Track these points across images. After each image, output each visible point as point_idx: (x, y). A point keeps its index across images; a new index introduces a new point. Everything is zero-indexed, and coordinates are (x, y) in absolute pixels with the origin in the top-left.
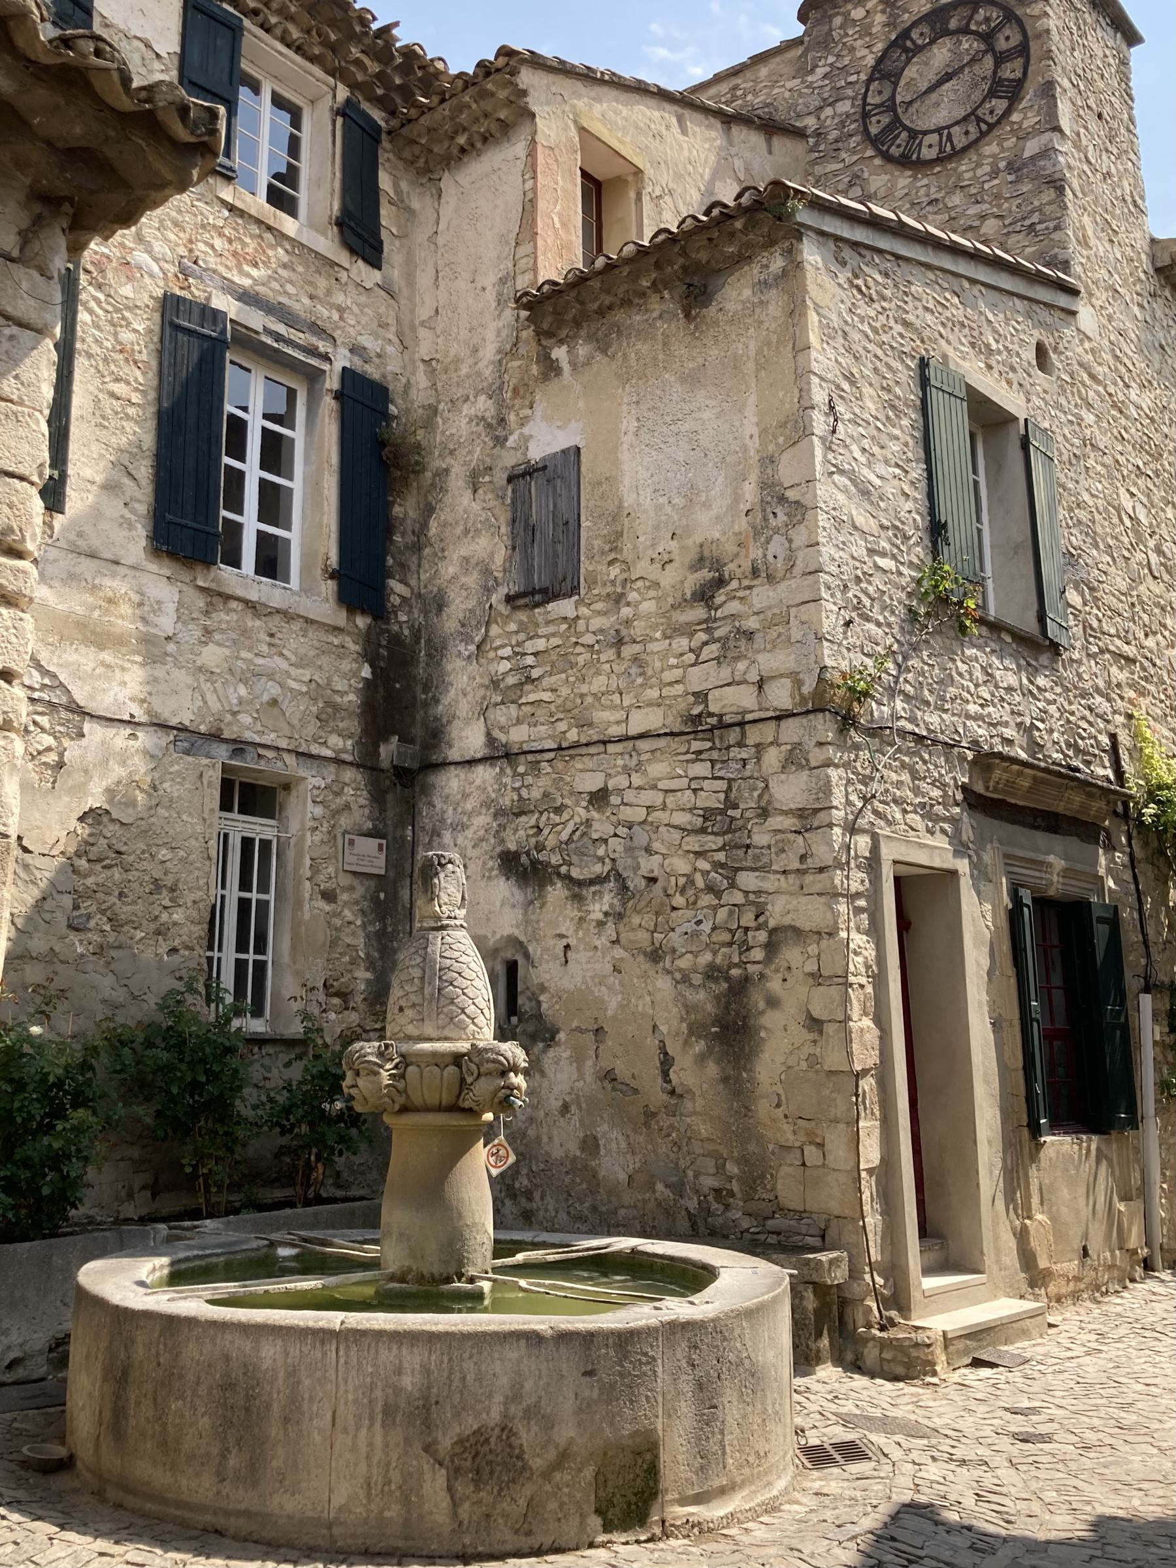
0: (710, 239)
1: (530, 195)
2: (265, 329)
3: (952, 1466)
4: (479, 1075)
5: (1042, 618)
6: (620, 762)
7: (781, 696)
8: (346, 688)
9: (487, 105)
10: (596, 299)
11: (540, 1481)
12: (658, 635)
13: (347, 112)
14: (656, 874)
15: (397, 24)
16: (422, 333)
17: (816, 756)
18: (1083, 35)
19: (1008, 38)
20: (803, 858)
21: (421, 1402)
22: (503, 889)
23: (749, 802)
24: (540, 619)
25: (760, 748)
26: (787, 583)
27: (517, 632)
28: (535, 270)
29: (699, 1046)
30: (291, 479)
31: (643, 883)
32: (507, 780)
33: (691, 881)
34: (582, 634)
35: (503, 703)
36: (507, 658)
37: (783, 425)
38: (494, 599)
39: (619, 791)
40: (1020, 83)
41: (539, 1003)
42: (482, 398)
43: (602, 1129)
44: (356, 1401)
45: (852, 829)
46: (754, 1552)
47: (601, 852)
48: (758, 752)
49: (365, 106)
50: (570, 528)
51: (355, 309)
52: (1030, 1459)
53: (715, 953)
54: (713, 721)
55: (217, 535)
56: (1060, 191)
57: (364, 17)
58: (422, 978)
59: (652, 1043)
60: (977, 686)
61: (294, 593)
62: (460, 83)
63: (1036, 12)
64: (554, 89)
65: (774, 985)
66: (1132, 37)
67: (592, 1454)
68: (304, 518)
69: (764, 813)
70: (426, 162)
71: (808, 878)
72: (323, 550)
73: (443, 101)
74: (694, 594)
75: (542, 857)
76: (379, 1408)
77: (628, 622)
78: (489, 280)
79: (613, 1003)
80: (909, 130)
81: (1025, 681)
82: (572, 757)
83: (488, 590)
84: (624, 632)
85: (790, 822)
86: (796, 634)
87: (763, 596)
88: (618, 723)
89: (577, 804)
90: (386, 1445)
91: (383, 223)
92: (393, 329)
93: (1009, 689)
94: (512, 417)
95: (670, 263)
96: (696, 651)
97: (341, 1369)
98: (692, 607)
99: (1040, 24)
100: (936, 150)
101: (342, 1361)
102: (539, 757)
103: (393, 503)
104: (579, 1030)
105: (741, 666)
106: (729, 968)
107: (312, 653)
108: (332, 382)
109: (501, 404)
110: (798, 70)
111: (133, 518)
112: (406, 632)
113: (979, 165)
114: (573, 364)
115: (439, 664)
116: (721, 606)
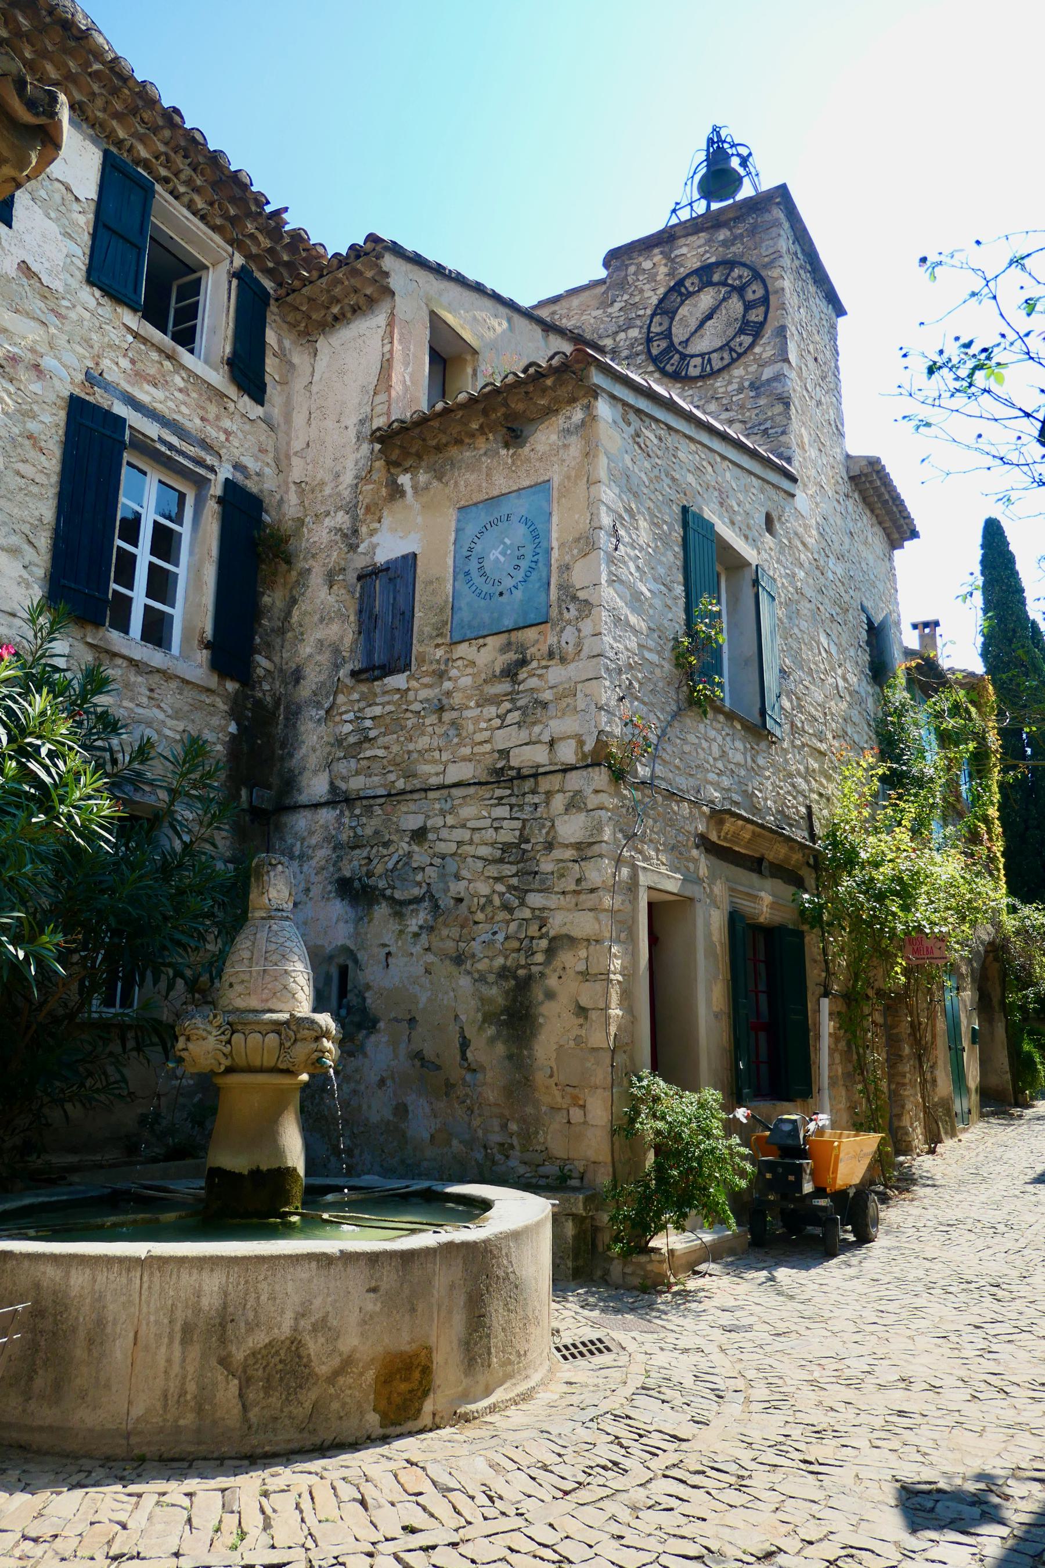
0: (526, 393)
1: (387, 356)
2: (160, 438)
3: (676, 1354)
4: (295, 1041)
5: (763, 713)
6: (437, 806)
7: (567, 753)
8: (214, 740)
9: (355, 282)
10: (435, 437)
11: (325, 1385)
12: (472, 704)
13: (241, 275)
14: (462, 895)
15: (286, 209)
16: (295, 461)
17: (593, 801)
18: (807, 300)
19: (754, 292)
20: (578, 881)
21: (218, 1321)
22: (338, 908)
23: (539, 837)
24: (378, 690)
25: (549, 794)
26: (575, 664)
27: (359, 701)
28: (388, 414)
29: (491, 1031)
30: (177, 565)
31: (452, 902)
32: (346, 820)
33: (489, 901)
34: (411, 703)
35: (345, 757)
36: (350, 722)
37: (577, 540)
38: (341, 673)
39: (436, 830)
40: (762, 324)
41: (364, 999)
42: (341, 513)
43: (410, 1099)
44: (156, 1322)
45: (619, 861)
46: (511, 1436)
47: (419, 878)
48: (548, 798)
49: (258, 274)
50: (406, 617)
51: (239, 433)
52: (736, 1346)
53: (506, 957)
54: (513, 773)
55: (107, 601)
56: (787, 405)
57: (261, 200)
58: (251, 959)
59: (453, 1029)
60: (715, 759)
61: (173, 657)
62: (335, 262)
63: (775, 275)
64: (411, 276)
65: (552, 982)
66: (840, 311)
67: (373, 1359)
68: (186, 599)
69: (550, 846)
70: (306, 326)
71: (583, 897)
72: (200, 625)
73: (321, 276)
74: (502, 671)
75: (371, 882)
76: (178, 1327)
77: (448, 694)
78: (352, 420)
79: (423, 999)
80: (681, 353)
81: (749, 760)
82: (399, 802)
83: (337, 667)
84: (445, 701)
85: (569, 854)
86: (581, 705)
87: (556, 674)
88: (437, 774)
89: (402, 840)
90: (184, 1360)
91: (268, 369)
92: (271, 455)
93: (738, 764)
94: (364, 530)
95: (494, 410)
96: (502, 717)
97: (145, 1293)
98: (500, 682)
99: (778, 284)
100: (699, 369)
101: (145, 1286)
102: (372, 802)
103: (263, 594)
104: (396, 1020)
105: (537, 729)
106: (517, 969)
107: (186, 708)
108: (216, 489)
109: (355, 519)
110: (602, 303)
111: (31, 579)
112: (268, 699)
113: (730, 383)
114: (415, 487)
115: (294, 726)
116: (523, 681)
